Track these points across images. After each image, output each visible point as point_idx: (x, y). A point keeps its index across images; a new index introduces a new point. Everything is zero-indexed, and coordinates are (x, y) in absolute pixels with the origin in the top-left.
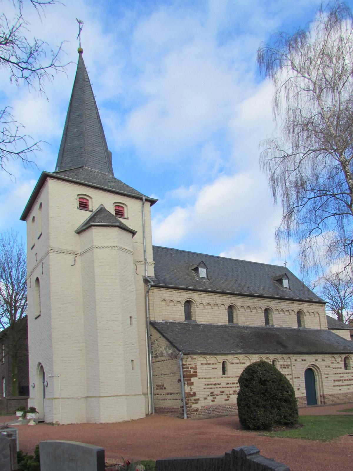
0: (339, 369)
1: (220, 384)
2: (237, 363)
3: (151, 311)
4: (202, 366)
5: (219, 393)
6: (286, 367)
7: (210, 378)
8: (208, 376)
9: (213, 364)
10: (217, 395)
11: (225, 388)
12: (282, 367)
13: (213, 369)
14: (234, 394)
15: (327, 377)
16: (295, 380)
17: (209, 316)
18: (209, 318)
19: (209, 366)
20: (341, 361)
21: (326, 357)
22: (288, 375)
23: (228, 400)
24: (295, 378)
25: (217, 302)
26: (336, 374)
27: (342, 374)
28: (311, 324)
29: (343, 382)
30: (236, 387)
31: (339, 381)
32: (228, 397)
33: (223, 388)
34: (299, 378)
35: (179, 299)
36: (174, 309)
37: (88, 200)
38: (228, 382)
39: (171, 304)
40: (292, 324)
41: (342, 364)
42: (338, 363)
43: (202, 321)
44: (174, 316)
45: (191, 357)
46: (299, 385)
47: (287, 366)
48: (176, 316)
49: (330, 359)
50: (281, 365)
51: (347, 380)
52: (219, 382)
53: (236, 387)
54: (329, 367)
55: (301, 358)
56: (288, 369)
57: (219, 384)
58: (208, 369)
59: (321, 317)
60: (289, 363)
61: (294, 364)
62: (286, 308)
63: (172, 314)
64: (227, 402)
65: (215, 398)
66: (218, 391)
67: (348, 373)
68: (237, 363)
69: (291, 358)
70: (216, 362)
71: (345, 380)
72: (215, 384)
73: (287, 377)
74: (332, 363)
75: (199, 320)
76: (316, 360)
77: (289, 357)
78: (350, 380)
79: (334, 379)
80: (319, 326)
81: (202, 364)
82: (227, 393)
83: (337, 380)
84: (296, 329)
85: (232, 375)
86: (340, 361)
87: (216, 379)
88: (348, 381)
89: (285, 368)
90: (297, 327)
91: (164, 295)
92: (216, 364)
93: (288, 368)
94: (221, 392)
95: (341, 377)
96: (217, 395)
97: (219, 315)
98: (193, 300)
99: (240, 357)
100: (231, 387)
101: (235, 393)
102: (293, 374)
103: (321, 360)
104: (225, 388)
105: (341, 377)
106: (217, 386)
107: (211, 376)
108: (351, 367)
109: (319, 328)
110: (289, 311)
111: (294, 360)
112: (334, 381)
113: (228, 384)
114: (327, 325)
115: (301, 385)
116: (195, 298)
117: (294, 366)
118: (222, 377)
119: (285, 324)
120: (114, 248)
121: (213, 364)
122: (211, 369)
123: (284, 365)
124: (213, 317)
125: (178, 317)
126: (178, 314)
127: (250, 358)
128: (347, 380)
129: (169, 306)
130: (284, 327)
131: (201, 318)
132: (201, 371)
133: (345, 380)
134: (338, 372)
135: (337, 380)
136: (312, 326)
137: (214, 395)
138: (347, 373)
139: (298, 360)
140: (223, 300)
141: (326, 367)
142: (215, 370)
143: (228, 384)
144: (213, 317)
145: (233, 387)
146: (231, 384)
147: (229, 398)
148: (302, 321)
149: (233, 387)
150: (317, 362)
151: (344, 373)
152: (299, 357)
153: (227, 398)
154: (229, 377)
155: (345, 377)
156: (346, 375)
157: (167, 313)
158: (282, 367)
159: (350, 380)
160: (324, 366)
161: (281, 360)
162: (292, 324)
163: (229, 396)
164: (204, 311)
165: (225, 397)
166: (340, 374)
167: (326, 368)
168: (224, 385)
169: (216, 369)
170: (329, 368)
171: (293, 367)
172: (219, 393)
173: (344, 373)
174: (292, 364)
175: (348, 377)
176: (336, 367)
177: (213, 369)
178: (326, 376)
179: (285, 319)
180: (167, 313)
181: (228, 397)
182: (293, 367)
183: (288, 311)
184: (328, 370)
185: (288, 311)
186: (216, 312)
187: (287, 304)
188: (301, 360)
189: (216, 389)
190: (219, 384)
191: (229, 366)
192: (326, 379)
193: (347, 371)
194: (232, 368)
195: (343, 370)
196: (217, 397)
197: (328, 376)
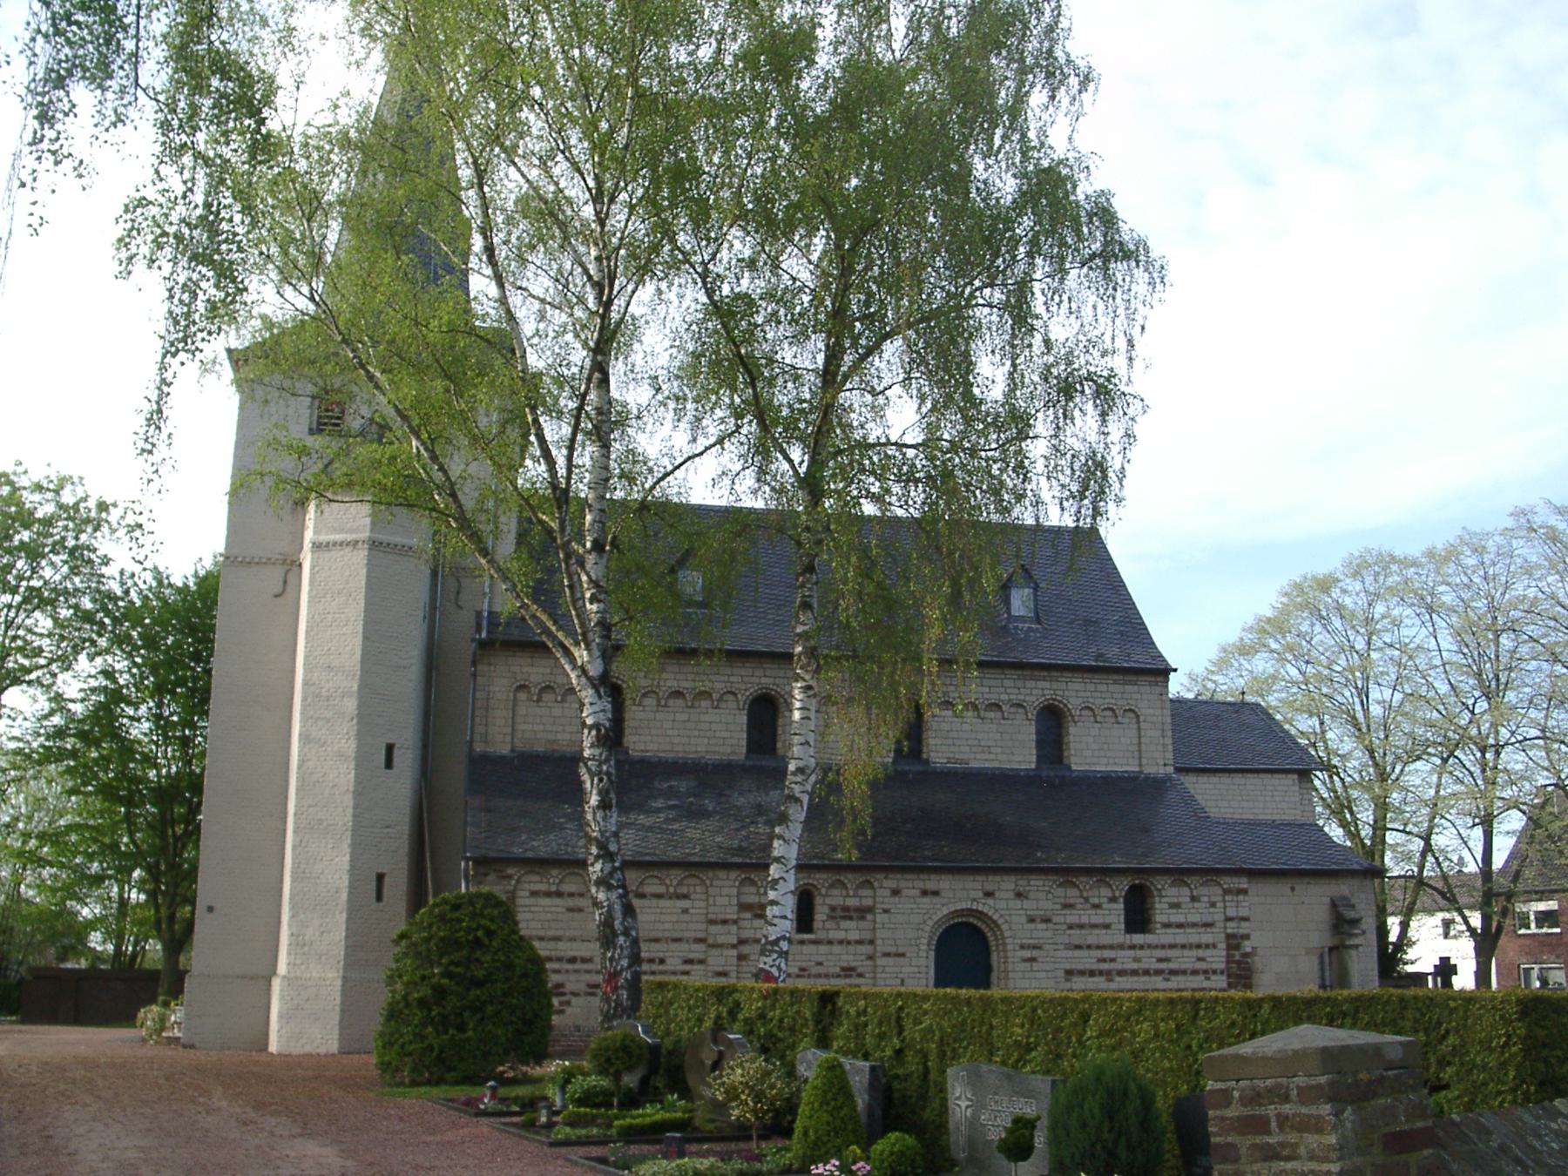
0: (1096, 931)
1: (662, 961)
3: (477, 720)
4: (533, 901)
5: (582, 987)
6: (853, 914)
7: (557, 939)
8: (551, 933)
9: (571, 895)
10: (576, 994)
12: (839, 913)
13: (571, 910)
15: (1032, 960)
16: (881, 961)
17: (676, 732)
18: (676, 740)
19: (558, 901)
20: (1113, 900)
21: (1032, 882)
22: (541, 939)
24: (887, 955)
26: (1078, 947)
27: (1112, 947)
28: (1102, 753)
29: (1208, 979)
31: (1092, 973)
34: (903, 955)
40: (1012, 754)
41: (1115, 914)
42: (1097, 906)
44: (551, 737)
45: (495, 871)
46: (899, 981)
47: (858, 910)
48: (559, 736)
49: (1060, 892)
50: (833, 909)
51: (1134, 973)
54: (1047, 920)
55: (920, 884)
56: (862, 924)
58: (553, 909)
60: (868, 902)
61: (885, 907)
62: (986, 696)
65: (568, 1003)
66: (578, 981)
67: (1142, 947)
69: (876, 884)
71: (1121, 973)
72: (573, 960)
73: (536, 944)
74: (1066, 906)
76: (989, 894)
77: (868, 882)
78: (1146, 972)
79: (1068, 966)
80: (1136, 762)
83: (1082, 973)
84: (1031, 773)
86: (1105, 900)
87: (576, 945)
88: (1135, 978)
89: (850, 918)
90: (1033, 766)
91: (525, 670)
93: (863, 918)
94: (590, 986)
95: (1160, 960)
96: (576, 994)
97: (714, 727)
99: (668, 876)
102: (879, 942)
103: (1011, 895)
105: (1160, 960)
106: (578, 966)
107: (559, 933)
108: (1158, 926)
109: (1137, 769)
110: (1000, 707)
111: (887, 893)
112: (1069, 973)
114: (1170, 755)
115: (906, 981)
117: (886, 911)
119: (978, 756)
121: (571, 895)
123: (846, 909)
124: (689, 737)
125: (567, 736)
126: (568, 729)
127: (708, 882)
128: (1134, 973)
130: (974, 764)
132: (530, 916)
133: (1121, 973)
134: (1091, 940)
135: (1082, 973)
136: (1104, 761)
137: (564, 994)
138: (1132, 947)
139: (905, 892)
141: (1032, 920)
142: (576, 915)
144: (689, 737)
150: (990, 901)
151: (1121, 947)
152: (911, 885)
155: (1125, 960)
156: (1131, 953)
158: (839, 913)
159: (1146, 972)
160: (1024, 919)
161: (836, 892)
162: (1012, 754)
164: (659, 716)
166: (1099, 947)
167: (1032, 926)
170: (1044, 926)
171: (880, 918)
172: (582, 987)
173: (1121, 947)
174: (878, 906)
175: (1137, 960)
176: (1085, 920)
177: (571, 910)
178: (1027, 954)
179: (980, 736)
182: (880, 918)
183: (996, 706)
184: (1041, 932)
185: (996, 706)
186: (703, 718)
187: (993, 683)
188: (917, 892)
189: (573, 977)
192: (1028, 965)
193: (1138, 938)
195: (1118, 935)
196: (574, 1000)
197: (1035, 953)
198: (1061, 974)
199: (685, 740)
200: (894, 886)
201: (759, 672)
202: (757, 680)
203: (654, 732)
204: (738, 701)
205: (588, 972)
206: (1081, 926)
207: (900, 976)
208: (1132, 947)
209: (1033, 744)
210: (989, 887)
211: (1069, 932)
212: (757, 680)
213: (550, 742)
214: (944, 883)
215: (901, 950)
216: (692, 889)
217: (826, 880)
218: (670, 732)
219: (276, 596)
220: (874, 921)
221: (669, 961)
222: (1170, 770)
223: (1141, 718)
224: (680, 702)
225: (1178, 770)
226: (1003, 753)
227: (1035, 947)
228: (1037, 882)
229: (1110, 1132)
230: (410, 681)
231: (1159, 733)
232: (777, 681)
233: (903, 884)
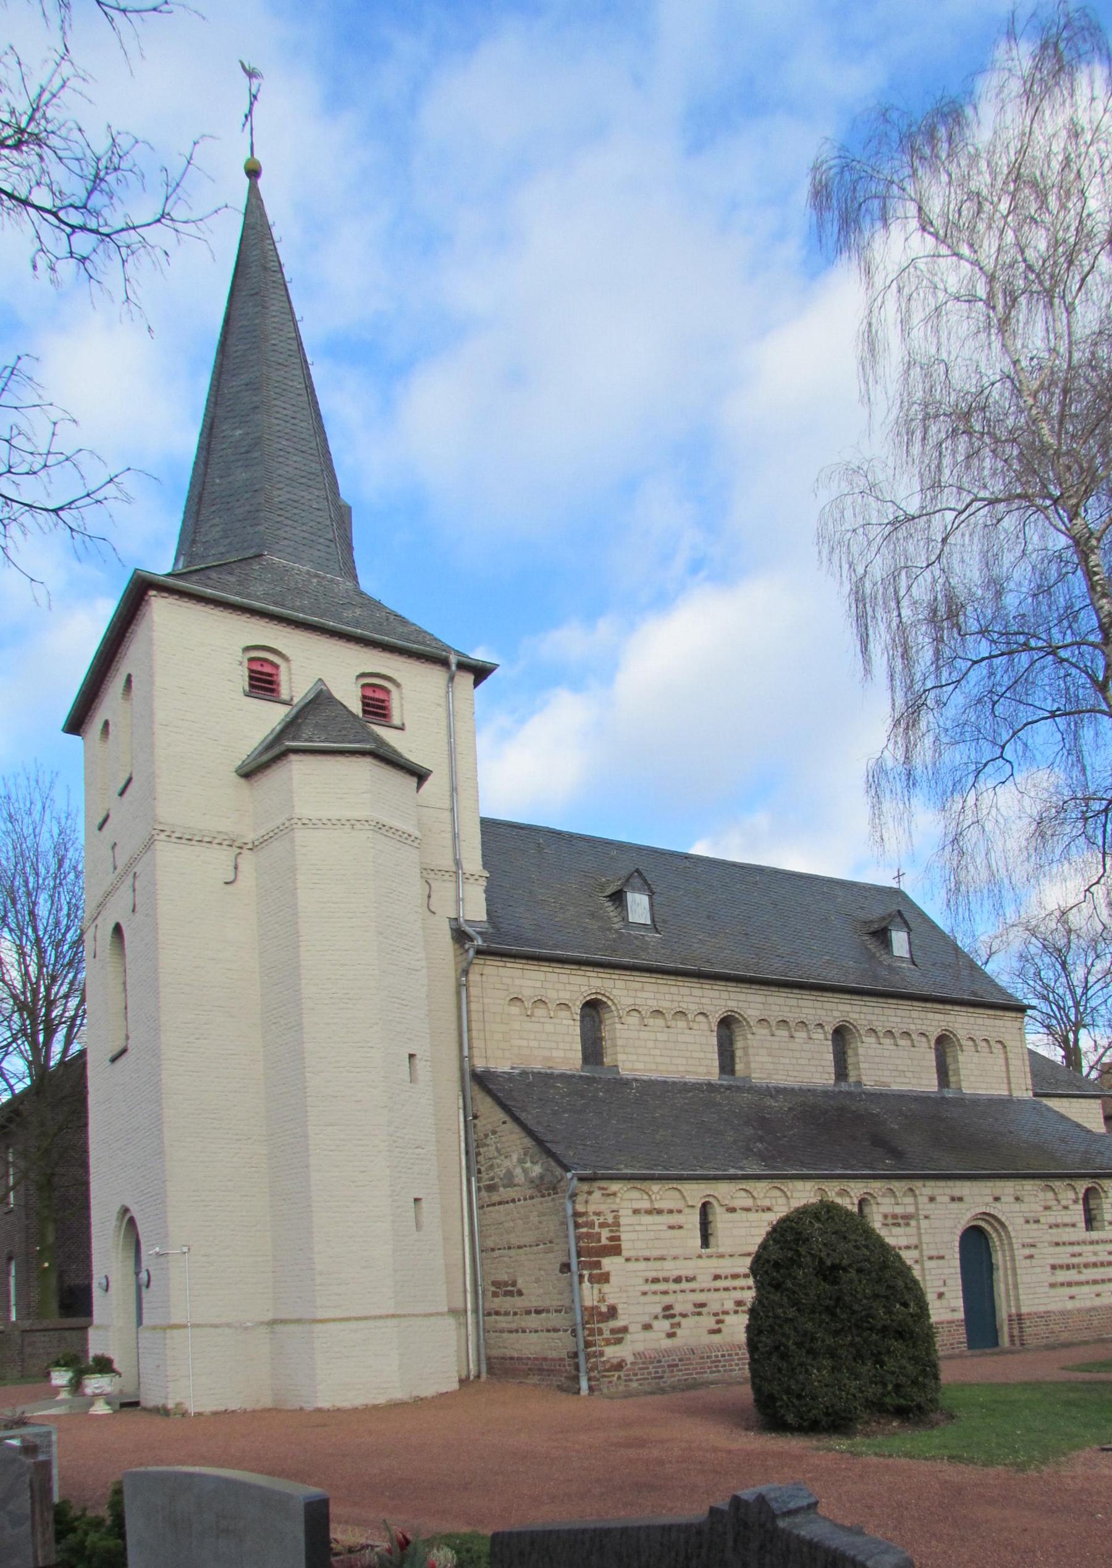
2: (748, 1210)
3: (474, 1034)
4: (635, 1219)
5: (690, 1308)
7: (662, 1258)
9: (671, 1212)
10: (684, 1316)
11: (709, 1290)
13: (671, 1227)
14: (736, 1312)
15: (1031, 1257)
16: (929, 1264)
17: (657, 1052)
18: (659, 1060)
20: (1076, 1202)
23: (719, 1331)
24: (931, 1258)
25: (684, 1005)
29: (1080, 1272)
30: (742, 1288)
32: (719, 1322)
33: (702, 1291)
34: (942, 1258)
35: (565, 996)
36: (549, 1028)
37: (277, 667)
38: (718, 1272)
39: (540, 1012)
41: (1077, 1213)
43: (635, 1070)
44: (547, 1053)
45: (600, 1189)
46: (942, 1283)
48: (555, 1054)
49: (1041, 1195)
50: (885, 1216)
51: (1095, 1265)
52: (690, 1273)
53: (742, 1288)
54: (1037, 1221)
55: (948, 1191)
56: (909, 1230)
57: (689, 1280)
58: (655, 1227)
59: (1010, 1055)
60: (911, 1209)
63: (543, 1044)
64: (716, 1338)
65: (679, 1325)
68: (748, 1210)
69: (917, 1192)
70: (680, 1205)
71: (1086, 1266)
72: (678, 1280)
75: (628, 1065)
76: (997, 1199)
77: (911, 1190)
78: (1102, 1264)
79: (1052, 1262)
80: (1005, 1086)
81: (636, 1212)
82: (715, 1307)
83: (1061, 1267)
85: (729, 1250)
86: (1070, 1202)
87: (680, 1263)
89: (899, 1225)
92: (680, 1211)
94: (696, 1305)
98: (604, 995)
99: (755, 1188)
100: (726, 1289)
101: (740, 1309)
102: (925, 1246)
104: (709, 1290)
106: (684, 1285)
107: (664, 1252)
108: (1106, 1223)
109: (1006, 1093)
111: (925, 1199)
112: (1053, 1267)
113: (717, 1277)
115: (947, 1281)
116: (615, 992)
117: (926, 1217)
118: (700, 1257)
120: (358, 826)
121: (671, 1212)
122: (665, 1228)
123: (895, 1216)
125: (561, 1054)
127: (789, 1194)
128: (1095, 1265)
129: (533, 1019)
130: (895, 1087)
131: (634, 1057)
132: (633, 1236)
133: (1086, 1266)
135: (1061, 1267)
136: (984, 1086)
137: (673, 1316)
138: (1092, 1243)
139: (939, 1199)
140: (703, 1000)
142: (676, 1232)
143: (717, 1277)
145: (735, 1288)
146: (726, 1278)
147: (720, 1325)
148: (951, 1067)
149: (735, 1288)
150: (998, 1205)
152: (943, 1190)
153: (716, 1327)
154: (721, 1256)
155: (1088, 1254)
157: (525, 1043)
158: (890, 1221)
159: (1102, 1264)
160: (1022, 1221)
163: (721, 1317)
165: (710, 1322)
166: (1072, 1244)
168: (704, 1281)
169: (680, 1227)
171: (924, 1223)
172: (690, 1308)
174: (920, 1212)
175: (1095, 1254)
177: (671, 1227)
180: (525, 1043)
181: (719, 1322)
182: (924, 1223)
183: (907, 1034)
185: (907, 1034)
186: (681, 1038)
188: (947, 1199)
189: (680, 1296)
190: (689, 1280)
191: (720, 1220)
192: (1028, 1261)
193: (1094, 1235)
194: (730, 1225)
197: (1032, 1251)
198: (1048, 1269)
199: (667, 1060)
200: (930, 1193)
201: (725, 995)
202: (723, 1003)
203: (640, 1051)
204: (709, 1023)
205: (693, 1291)
206: (1057, 1226)
207: (942, 1277)
208: (1092, 1243)
209: (935, 1070)
210: (957, 1193)
211: (1050, 1231)
212: (723, 1003)
213: (546, 1058)
214: (963, 1188)
215: (941, 1254)
216: (774, 1202)
217: (880, 1189)
218: (653, 1052)
219: (226, 883)
220: (919, 1228)
221: (699, 1278)
222: (1030, 1093)
223: (1008, 1049)
224: (660, 1022)
225: (1036, 1095)
226: (914, 1077)
227: (1033, 1246)
228: (1029, 1185)
229: (68, 1461)
230: (423, 985)
231: (1021, 1063)
232: (740, 1004)
233: (936, 1192)
